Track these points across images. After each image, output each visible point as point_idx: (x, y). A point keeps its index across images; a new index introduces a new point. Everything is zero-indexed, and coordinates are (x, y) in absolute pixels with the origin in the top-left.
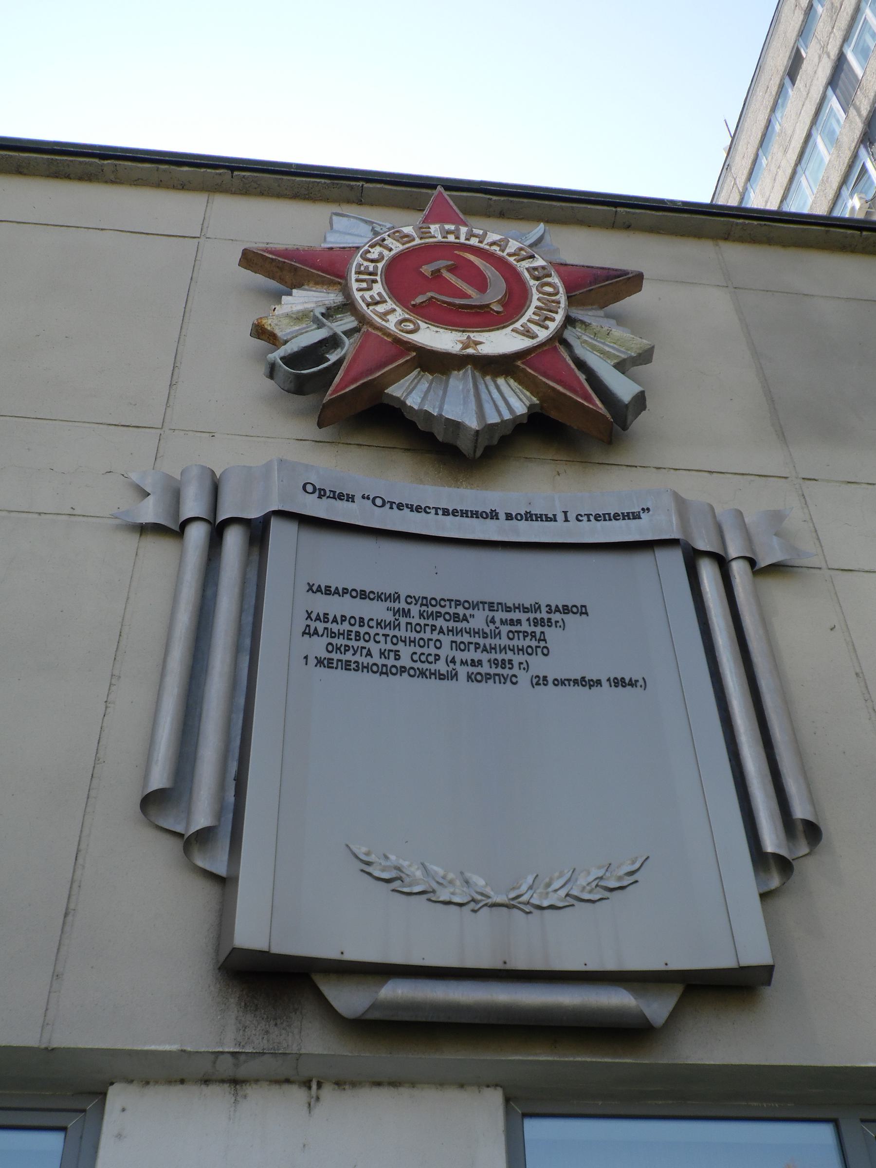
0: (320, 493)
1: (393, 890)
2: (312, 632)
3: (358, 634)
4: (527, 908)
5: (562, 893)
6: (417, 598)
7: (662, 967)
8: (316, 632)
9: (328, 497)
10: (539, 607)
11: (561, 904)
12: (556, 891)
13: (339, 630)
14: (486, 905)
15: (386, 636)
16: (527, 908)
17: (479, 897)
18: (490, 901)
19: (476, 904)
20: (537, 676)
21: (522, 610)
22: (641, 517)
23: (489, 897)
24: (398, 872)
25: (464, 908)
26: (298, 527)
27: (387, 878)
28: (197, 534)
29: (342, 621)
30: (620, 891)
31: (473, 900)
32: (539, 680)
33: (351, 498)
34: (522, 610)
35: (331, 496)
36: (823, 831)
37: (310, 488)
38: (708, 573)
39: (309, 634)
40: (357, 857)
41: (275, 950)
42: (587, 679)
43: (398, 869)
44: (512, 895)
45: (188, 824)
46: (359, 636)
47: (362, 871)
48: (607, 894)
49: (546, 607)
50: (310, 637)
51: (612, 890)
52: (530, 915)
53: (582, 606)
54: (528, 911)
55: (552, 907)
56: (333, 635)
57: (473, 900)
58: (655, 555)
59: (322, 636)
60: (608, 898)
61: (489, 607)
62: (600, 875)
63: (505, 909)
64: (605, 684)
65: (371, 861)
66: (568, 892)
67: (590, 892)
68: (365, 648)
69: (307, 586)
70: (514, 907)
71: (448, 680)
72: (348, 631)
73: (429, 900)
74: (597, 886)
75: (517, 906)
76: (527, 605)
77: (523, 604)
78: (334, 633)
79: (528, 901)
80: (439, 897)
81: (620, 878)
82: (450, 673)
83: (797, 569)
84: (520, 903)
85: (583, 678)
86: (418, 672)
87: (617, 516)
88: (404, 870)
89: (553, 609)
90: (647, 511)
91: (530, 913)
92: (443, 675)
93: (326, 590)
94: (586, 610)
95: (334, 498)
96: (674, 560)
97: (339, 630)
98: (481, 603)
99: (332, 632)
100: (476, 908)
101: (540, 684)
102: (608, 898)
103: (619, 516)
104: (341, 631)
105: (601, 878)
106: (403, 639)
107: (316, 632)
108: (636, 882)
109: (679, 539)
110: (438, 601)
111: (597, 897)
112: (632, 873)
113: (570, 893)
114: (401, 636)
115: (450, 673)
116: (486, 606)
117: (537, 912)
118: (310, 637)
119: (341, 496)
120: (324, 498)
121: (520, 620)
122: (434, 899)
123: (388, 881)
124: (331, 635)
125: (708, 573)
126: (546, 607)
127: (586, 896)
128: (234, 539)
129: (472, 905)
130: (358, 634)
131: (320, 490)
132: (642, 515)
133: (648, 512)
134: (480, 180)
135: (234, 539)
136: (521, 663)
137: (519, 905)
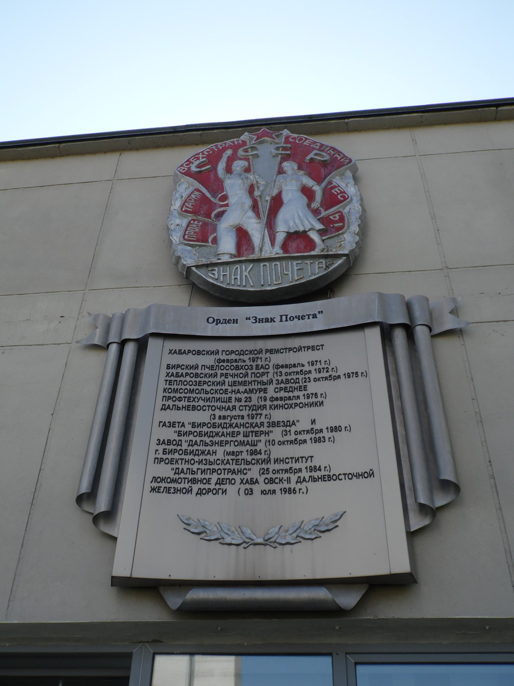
2: (302, 481)
3: (329, 476)
5: (295, 535)
8: (169, 407)
9: (222, 323)
11: (293, 542)
12: (291, 534)
13: (318, 476)
14: (251, 544)
15: (209, 406)
17: (248, 540)
22: (317, 316)
23: (253, 540)
24: (204, 528)
25: (239, 547)
27: (197, 532)
28: (114, 348)
29: (188, 353)
35: (224, 322)
37: (211, 320)
38: (399, 336)
39: (300, 482)
41: (135, 575)
43: (204, 527)
45: (95, 510)
46: (330, 477)
47: (185, 529)
48: (320, 534)
50: (301, 484)
52: (276, 549)
54: (274, 546)
55: (288, 543)
56: (315, 480)
57: (244, 542)
59: (308, 482)
62: (316, 523)
63: (262, 546)
64: (309, 441)
65: (189, 523)
66: (298, 534)
67: (310, 534)
72: (188, 406)
73: (220, 543)
74: (315, 530)
78: (316, 478)
80: (225, 542)
81: (327, 525)
84: (271, 542)
90: (321, 313)
95: (225, 323)
96: (375, 334)
97: (318, 476)
99: (314, 478)
100: (245, 547)
102: (321, 537)
103: (231, 321)
104: (184, 406)
105: (317, 525)
106: (219, 407)
107: (169, 407)
108: (337, 526)
110: (225, 367)
111: (313, 537)
112: (336, 521)
114: (217, 406)
116: (186, 399)
118: (301, 484)
123: (199, 534)
124: (314, 480)
125: (399, 336)
127: (308, 536)
129: (245, 545)
130: (329, 476)
131: (217, 320)
132: (318, 316)
134: (185, 124)
135: (130, 350)
136: (330, 438)
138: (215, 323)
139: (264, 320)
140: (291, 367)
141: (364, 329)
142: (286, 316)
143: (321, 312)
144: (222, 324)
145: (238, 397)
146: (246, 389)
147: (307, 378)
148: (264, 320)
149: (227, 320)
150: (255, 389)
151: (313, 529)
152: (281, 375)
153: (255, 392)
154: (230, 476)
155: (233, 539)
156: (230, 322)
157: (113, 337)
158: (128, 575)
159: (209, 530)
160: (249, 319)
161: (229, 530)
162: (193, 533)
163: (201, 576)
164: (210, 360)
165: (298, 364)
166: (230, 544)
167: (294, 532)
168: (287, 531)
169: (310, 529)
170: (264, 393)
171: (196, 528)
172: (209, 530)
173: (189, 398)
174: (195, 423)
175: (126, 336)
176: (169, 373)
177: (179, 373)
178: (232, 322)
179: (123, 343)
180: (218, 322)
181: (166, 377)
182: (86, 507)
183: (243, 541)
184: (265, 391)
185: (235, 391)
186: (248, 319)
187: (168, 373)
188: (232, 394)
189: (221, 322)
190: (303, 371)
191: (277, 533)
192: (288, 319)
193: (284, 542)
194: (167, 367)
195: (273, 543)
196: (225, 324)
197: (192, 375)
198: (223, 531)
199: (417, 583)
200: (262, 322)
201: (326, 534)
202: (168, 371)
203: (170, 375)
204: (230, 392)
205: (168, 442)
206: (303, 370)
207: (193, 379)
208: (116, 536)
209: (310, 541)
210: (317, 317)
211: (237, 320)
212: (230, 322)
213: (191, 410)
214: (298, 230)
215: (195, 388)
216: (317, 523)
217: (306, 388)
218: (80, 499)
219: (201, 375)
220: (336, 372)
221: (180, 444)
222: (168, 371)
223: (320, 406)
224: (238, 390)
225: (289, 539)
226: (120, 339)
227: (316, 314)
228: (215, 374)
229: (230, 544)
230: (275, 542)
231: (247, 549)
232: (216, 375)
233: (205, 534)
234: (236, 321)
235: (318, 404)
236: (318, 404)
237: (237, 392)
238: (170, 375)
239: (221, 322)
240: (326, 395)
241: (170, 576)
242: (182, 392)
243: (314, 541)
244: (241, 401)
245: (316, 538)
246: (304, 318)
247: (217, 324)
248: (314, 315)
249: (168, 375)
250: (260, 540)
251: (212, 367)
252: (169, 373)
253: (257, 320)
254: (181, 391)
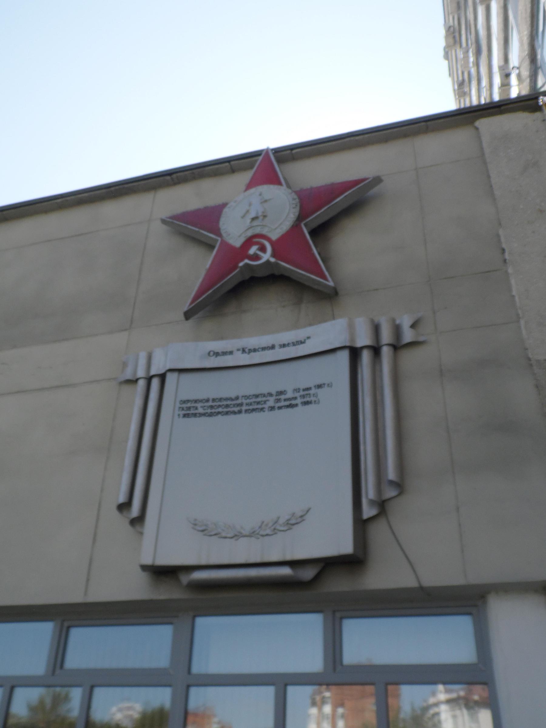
12: (270, 527)
16: (259, 536)
28: (142, 383)
33: (231, 353)
37: (212, 353)
55: (267, 535)
96: (344, 357)
108: (304, 520)
125: (366, 357)
128: (155, 383)
135: (155, 383)
154: (193, 405)
157: (141, 373)
163: (203, 562)
166: (225, 538)
168: (267, 525)
175: (153, 372)
179: (149, 379)
186: (238, 350)
201: (296, 526)
214: (527, 57)
225: (268, 531)
229: (225, 538)
230: (258, 534)
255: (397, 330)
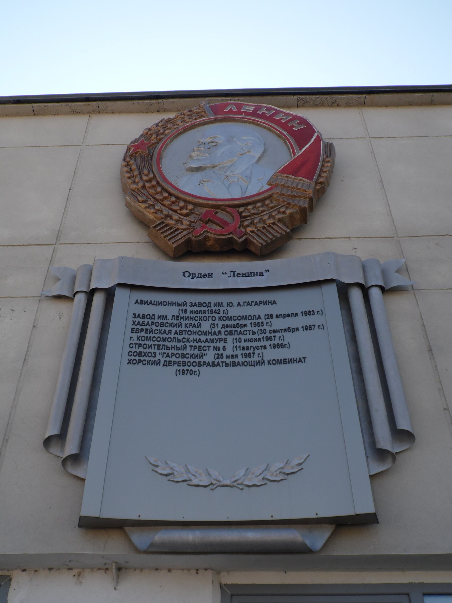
0: (192, 276)
1: (169, 480)
4: (241, 487)
5: (261, 477)
6: (254, 347)
7: (315, 516)
9: (198, 277)
10: (186, 304)
16: (241, 487)
18: (220, 484)
19: (214, 486)
20: (268, 315)
21: (176, 305)
24: (172, 470)
26: (130, 290)
28: (81, 299)
30: (292, 475)
31: (212, 484)
32: (269, 317)
34: (176, 305)
35: (200, 276)
36: (415, 436)
37: (187, 274)
40: (151, 463)
42: (291, 328)
43: (172, 469)
44: (233, 480)
47: (153, 470)
48: (286, 477)
49: (190, 303)
51: (288, 474)
52: (243, 490)
53: (209, 303)
54: (241, 488)
55: (254, 485)
57: (212, 484)
58: (322, 290)
60: (286, 479)
61: (158, 347)
64: (268, 347)
67: (276, 476)
68: (166, 353)
69: (208, 367)
70: (235, 486)
71: (181, 350)
73: (188, 485)
74: (280, 473)
75: (236, 486)
76: (180, 302)
77: (177, 302)
79: (242, 483)
81: (292, 468)
82: (182, 347)
83: (421, 290)
84: (238, 484)
85: (289, 328)
86: (147, 354)
87: (239, 275)
88: (174, 468)
89: (193, 304)
90: (267, 271)
91: (242, 489)
92: (179, 348)
93: (212, 364)
94: (210, 305)
95: (201, 277)
96: (332, 290)
97: (172, 345)
98: (153, 345)
100: (213, 488)
101: (219, 358)
102: (286, 479)
103: (240, 275)
105: (282, 468)
108: (302, 469)
109: (335, 279)
111: (278, 479)
112: (300, 464)
113: (265, 477)
115: (182, 347)
116: (156, 347)
117: (246, 489)
119: (205, 275)
120: (195, 278)
121: (298, 328)
122: (190, 484)
123: (167, 475)
126: (190, 303)
129: (211, 487)
131: (193, 274)
132: (265, 274)
133: (268, 272)
137: (237, 485)
138: (191, 277)
139: (259, 274)
140: (286, 317)
141: (321, 286)
142: (234, 272)
143: (267, 271)
144: (198, 278)
145: (217, 346)
146: (207, 339)
147: (272, 336)
148: (259, 274)
149: (202, 275)
150: (215, 338)
151: (278, 472)
152: (214, 327)
153: (215, 341)
155: (201, 481)
156: (239, 276)
158: (98, 516)
159: (177, 472)
160: (226, 274)
161: (196, 472)
162: (162, 474)
164: (175, 310)
165: (292, 314)
167: (260, 474)
169: (276, 472)
170: (224, 342)
171: (164, 470)
172: (177, 472)
173: (159, 346)
174: (286, 359)
176: (136, 321)
177: (145, 322)
178: (241, 276)
179: (91, 294)
180: (194, 276)
181: (132, 325)
182: (55, 449)
183: (210, 483)
184: (225, 340)
185: (196, 340)
187: (134, 321)
188: (193, 342)
189: (197, 276)
190: (240, 324)
191: (244, 475)
192: (236, 276)
193: (250, 484)
194: (132, 330)
195: (240, 485)
196: (200, 278)
197: (157, 324)
198: (191, 473)
199: (378, 522)
200: (251, 276)
202: (134, 320)
203: (136, 323)
204: (191, 341)
205: (180, 333)
206: (239, 323)
207: (159, 328)
208: (85, 478)
209: (276, 483)
210: (263, 275)
211: (212, 274)
212: (239, 276)
213: (181, 365)
215: (167, 336)
216: (281, 465)
217: (227, 340)
218: (48, 442)
219: (167, 325)
220: (271, 327)
221: (153, 317)
222: (134, 320)
223: (152, 365)
224: (200, 339)
226: (89, 289)
227: (262, 272)
228: (180, 324)
230: (242, 484)
231: (214, 490)
232: (180, 325)
233: (172, 476)
234: (210, 275)
235: (151, 362)
236: (151, 362)
237: (199, 341)
238: (136, 323)
239: (197, 276)
240: (233, 349)
241: (139, 516)
242: (155, 340)
243: (280, 482)
244: (219, 350)
245: (282, 480)
246: (206, 276)
247: (192, 278)
248: (261, 273)
249: (134, 323)
250: (228, 482)
251: (177, 318)
252: (136, 321)
253: (234, 274)
254: (154, 339)
255: (384, 273)
